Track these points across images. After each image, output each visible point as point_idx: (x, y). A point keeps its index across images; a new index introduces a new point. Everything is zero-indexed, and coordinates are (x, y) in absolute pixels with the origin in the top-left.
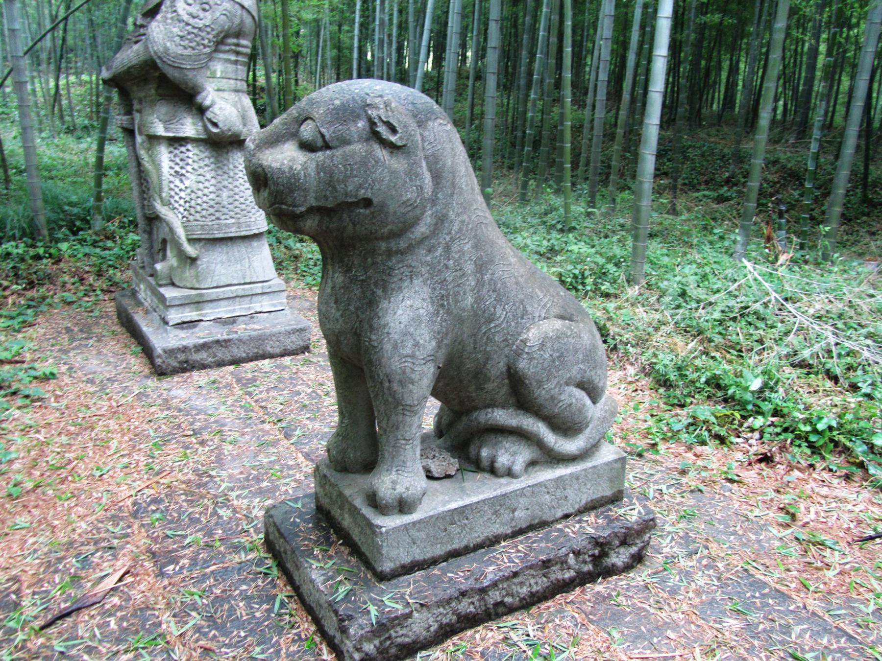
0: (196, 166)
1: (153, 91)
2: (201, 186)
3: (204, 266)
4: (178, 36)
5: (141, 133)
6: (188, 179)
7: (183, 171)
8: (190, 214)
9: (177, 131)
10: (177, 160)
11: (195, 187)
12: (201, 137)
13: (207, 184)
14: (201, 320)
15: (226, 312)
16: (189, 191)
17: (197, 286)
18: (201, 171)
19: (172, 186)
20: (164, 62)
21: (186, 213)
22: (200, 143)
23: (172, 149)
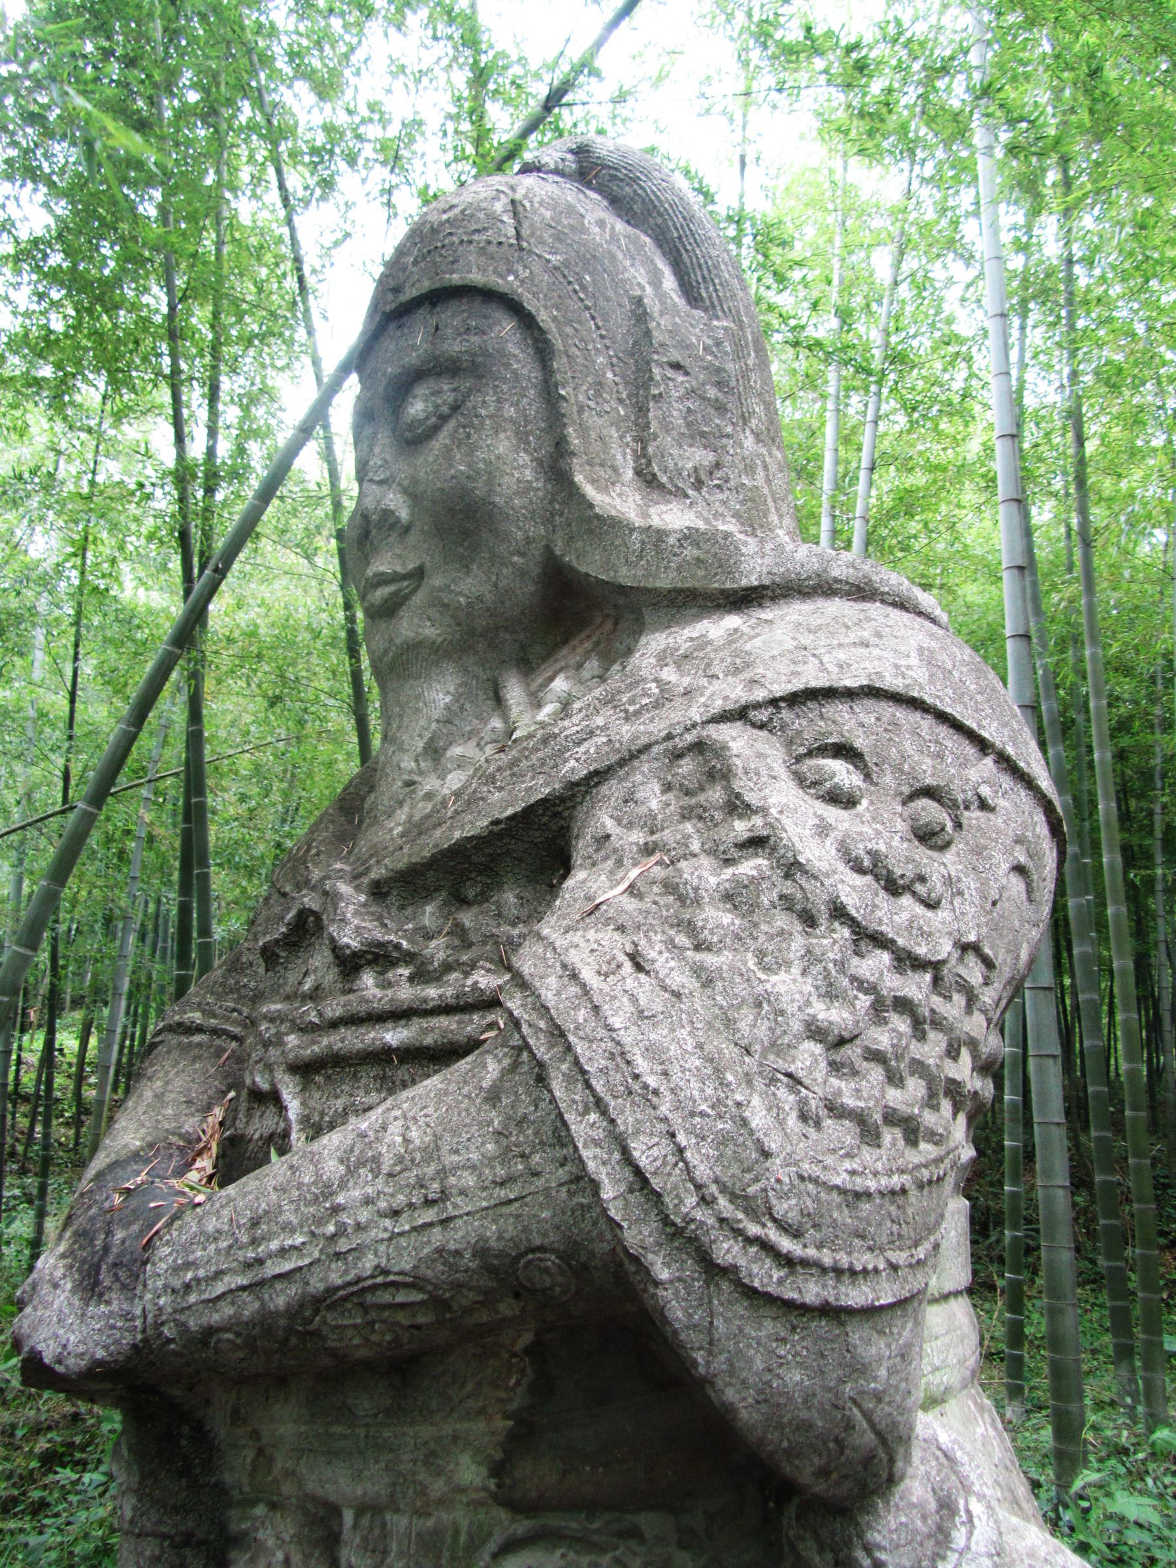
4: (815, 1032)
20: (712, 1270)
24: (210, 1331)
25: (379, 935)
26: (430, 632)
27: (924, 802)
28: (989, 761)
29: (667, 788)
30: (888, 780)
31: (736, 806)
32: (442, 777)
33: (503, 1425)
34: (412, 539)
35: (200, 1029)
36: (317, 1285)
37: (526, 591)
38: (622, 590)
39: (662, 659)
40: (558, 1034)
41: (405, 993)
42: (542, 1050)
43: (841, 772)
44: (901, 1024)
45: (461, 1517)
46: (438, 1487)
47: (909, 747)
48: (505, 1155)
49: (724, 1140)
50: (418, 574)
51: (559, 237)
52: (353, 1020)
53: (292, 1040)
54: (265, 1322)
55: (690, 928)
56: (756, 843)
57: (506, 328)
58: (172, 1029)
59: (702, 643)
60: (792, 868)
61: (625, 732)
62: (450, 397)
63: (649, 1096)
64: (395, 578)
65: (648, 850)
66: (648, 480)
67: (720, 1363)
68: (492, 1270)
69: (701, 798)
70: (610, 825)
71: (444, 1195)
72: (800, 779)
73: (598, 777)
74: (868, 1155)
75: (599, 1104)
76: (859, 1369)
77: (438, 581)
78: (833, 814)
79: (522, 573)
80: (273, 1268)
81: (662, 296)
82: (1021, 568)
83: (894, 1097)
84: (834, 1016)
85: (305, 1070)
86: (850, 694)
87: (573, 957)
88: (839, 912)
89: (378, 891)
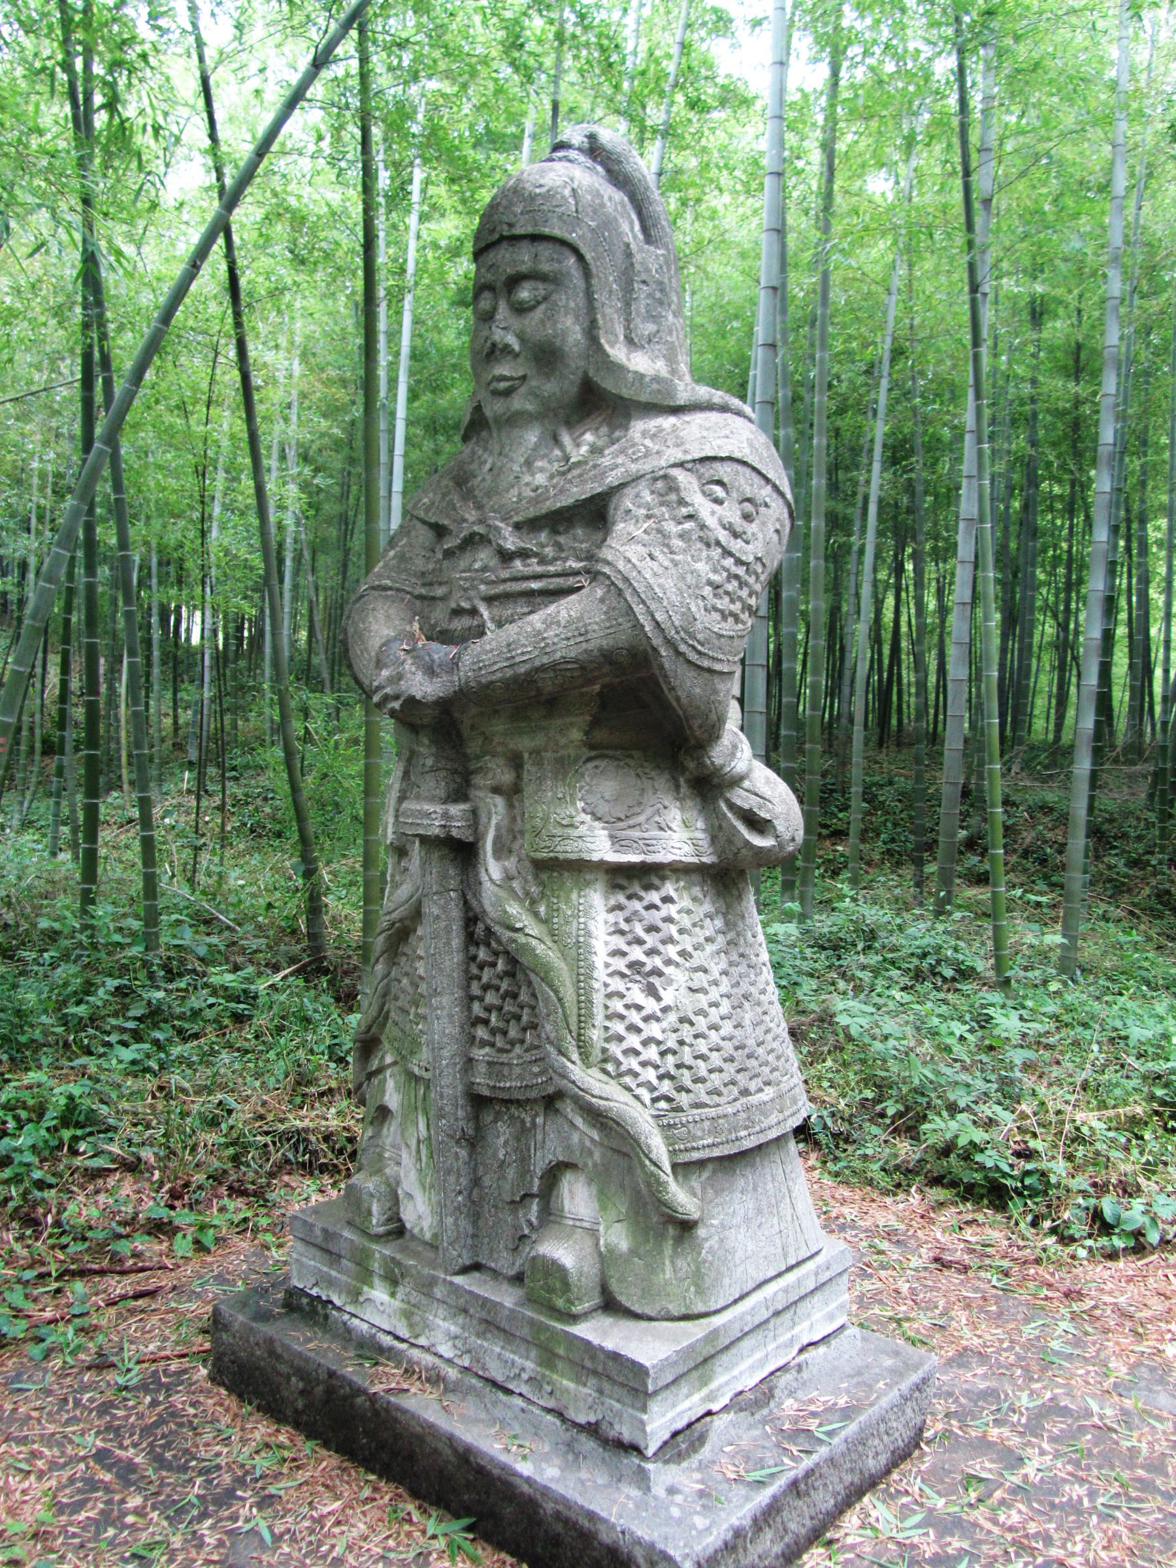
0: (687, 943)
1: (576, 735)
2: (703, 1000)
3: (713, 1242)
4: (710, 583)
5: (501, 851)
6: (670, 982)
7: (657, 961)
8: (680, 1089)
9: (648, 847)
10: (639, 930)
11: (688, 1004)
12: (706, 860)
13: (714, 993)
14: (709, 1413)
15: (752, 1369)
16: (672, 1017)
17: (700, 1308)
18: (699, 958)
19: (617, 1006)
20: (678, 653)
21: (666, 1087)
22: (695, 877)
23: (621, 898)
24: (492, 682)
25: (523, 545)
26: (530, 407)
27: (746, 504)
28: (769, 487)
29: (652, 492)
30: (734, 495)
31: (682, 502)
32: (533, 475)
33: (588, 718)
34: (520, 360)
35: (390, 589)
36: (537, 663)
37: (574, 390)
38: (622, 398)
39: (644, 434)
40: (626, 580)
41: (539, 569)
42: (620, 585)
43: (719, 491)
44: (735, 583)
45: (572, 752)
46: (563, 741)
47: (742, 481)
48: (609, 619)
49: (683, 614)
50: (524, 378)
51: (595, 212)
52: (515, 579)
53: (482, 587)
54: (515, 679)
55: (668, 546)
56: (690, 517)
57: (572, 260)
58: (373, 588)
59: (660, 429)
60: (703, 527)
61: (633, 467)
62: (543, 292)
63: (660, 600)
64: (512, 379)
65: (649, 517)
66: (630, 341)
67: (678, 683)
68: (604, 656)
69: (668, 498)
70: (631, 506)
71: (587, 632)
72: (704, 493)
73: (623, 486)
74: (723, 624)
75: (643, 602)
76: (715, 692)
77: (534, 383)
78: (716, 507)
79: (572, 382)
80: (518, 660)
81: (635, 237)
82: (774, 289)
83: (732, 607)
84: (716, 578)
85: (489, 600)
86: (722, 459)
87: (628, 554)
88: (718, 543)
89: (518, 526)
